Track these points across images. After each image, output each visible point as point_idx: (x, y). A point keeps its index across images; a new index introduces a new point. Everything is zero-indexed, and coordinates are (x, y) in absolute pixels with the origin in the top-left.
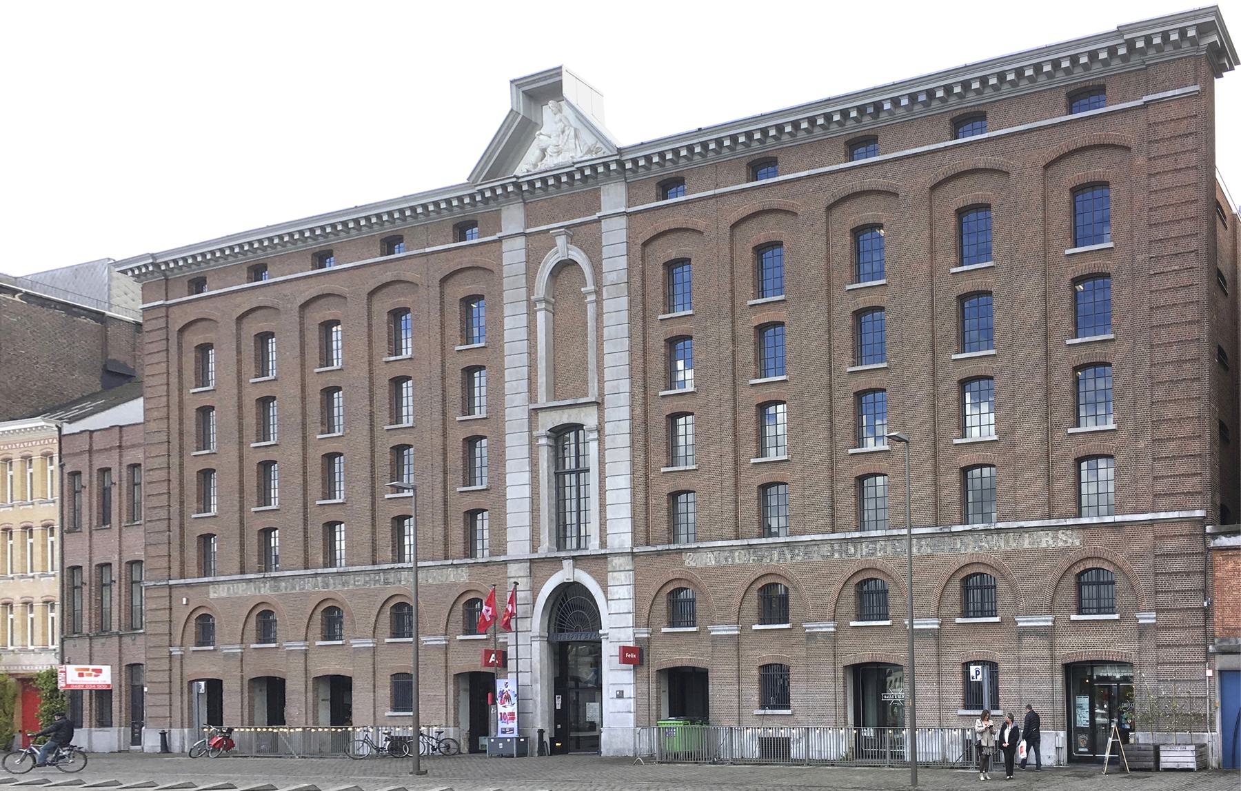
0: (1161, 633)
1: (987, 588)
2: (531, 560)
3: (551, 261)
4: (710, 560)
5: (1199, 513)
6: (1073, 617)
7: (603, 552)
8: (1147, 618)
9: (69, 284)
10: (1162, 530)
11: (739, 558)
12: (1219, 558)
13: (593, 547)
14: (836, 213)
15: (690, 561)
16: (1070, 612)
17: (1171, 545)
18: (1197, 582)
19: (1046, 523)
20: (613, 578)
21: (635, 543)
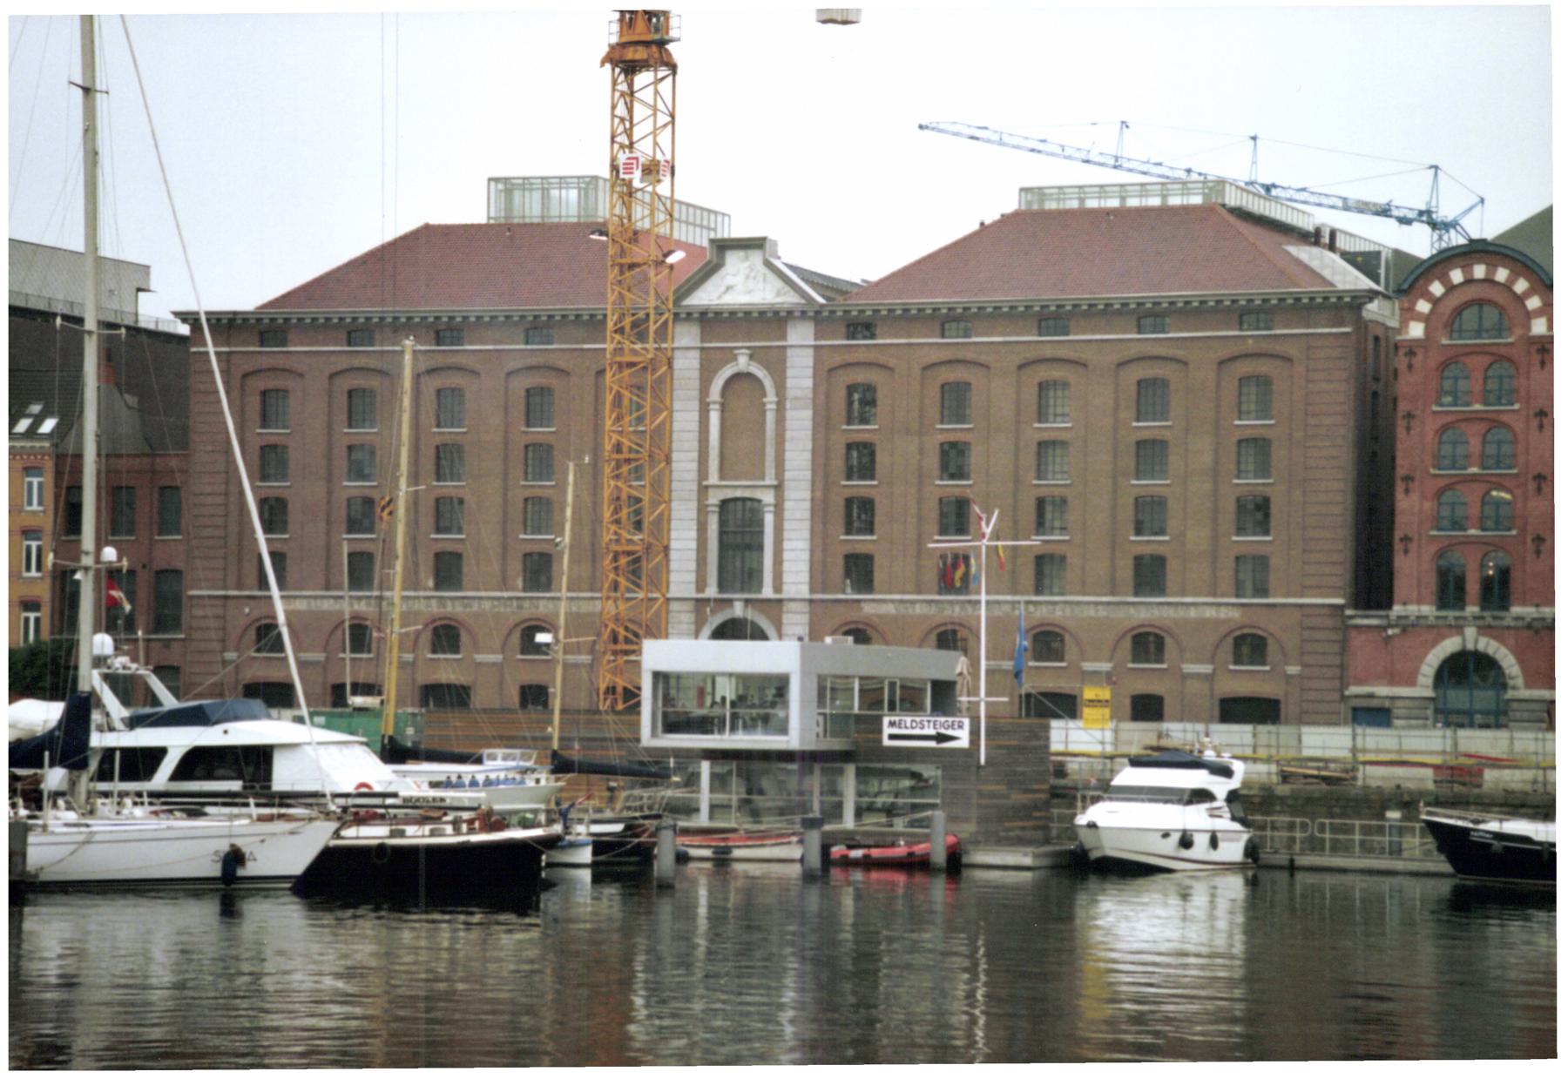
2: (698, 600)
3: (727, 372)
5: (1340, 601)
8: (1293, 669)
11: (919, 609)
12: (1353, 634)
13: (768, 592)
14: (1028, 371)
15: (868, 609)
17: (1314, 622)
20: (786, 618)
21: (812, 590)
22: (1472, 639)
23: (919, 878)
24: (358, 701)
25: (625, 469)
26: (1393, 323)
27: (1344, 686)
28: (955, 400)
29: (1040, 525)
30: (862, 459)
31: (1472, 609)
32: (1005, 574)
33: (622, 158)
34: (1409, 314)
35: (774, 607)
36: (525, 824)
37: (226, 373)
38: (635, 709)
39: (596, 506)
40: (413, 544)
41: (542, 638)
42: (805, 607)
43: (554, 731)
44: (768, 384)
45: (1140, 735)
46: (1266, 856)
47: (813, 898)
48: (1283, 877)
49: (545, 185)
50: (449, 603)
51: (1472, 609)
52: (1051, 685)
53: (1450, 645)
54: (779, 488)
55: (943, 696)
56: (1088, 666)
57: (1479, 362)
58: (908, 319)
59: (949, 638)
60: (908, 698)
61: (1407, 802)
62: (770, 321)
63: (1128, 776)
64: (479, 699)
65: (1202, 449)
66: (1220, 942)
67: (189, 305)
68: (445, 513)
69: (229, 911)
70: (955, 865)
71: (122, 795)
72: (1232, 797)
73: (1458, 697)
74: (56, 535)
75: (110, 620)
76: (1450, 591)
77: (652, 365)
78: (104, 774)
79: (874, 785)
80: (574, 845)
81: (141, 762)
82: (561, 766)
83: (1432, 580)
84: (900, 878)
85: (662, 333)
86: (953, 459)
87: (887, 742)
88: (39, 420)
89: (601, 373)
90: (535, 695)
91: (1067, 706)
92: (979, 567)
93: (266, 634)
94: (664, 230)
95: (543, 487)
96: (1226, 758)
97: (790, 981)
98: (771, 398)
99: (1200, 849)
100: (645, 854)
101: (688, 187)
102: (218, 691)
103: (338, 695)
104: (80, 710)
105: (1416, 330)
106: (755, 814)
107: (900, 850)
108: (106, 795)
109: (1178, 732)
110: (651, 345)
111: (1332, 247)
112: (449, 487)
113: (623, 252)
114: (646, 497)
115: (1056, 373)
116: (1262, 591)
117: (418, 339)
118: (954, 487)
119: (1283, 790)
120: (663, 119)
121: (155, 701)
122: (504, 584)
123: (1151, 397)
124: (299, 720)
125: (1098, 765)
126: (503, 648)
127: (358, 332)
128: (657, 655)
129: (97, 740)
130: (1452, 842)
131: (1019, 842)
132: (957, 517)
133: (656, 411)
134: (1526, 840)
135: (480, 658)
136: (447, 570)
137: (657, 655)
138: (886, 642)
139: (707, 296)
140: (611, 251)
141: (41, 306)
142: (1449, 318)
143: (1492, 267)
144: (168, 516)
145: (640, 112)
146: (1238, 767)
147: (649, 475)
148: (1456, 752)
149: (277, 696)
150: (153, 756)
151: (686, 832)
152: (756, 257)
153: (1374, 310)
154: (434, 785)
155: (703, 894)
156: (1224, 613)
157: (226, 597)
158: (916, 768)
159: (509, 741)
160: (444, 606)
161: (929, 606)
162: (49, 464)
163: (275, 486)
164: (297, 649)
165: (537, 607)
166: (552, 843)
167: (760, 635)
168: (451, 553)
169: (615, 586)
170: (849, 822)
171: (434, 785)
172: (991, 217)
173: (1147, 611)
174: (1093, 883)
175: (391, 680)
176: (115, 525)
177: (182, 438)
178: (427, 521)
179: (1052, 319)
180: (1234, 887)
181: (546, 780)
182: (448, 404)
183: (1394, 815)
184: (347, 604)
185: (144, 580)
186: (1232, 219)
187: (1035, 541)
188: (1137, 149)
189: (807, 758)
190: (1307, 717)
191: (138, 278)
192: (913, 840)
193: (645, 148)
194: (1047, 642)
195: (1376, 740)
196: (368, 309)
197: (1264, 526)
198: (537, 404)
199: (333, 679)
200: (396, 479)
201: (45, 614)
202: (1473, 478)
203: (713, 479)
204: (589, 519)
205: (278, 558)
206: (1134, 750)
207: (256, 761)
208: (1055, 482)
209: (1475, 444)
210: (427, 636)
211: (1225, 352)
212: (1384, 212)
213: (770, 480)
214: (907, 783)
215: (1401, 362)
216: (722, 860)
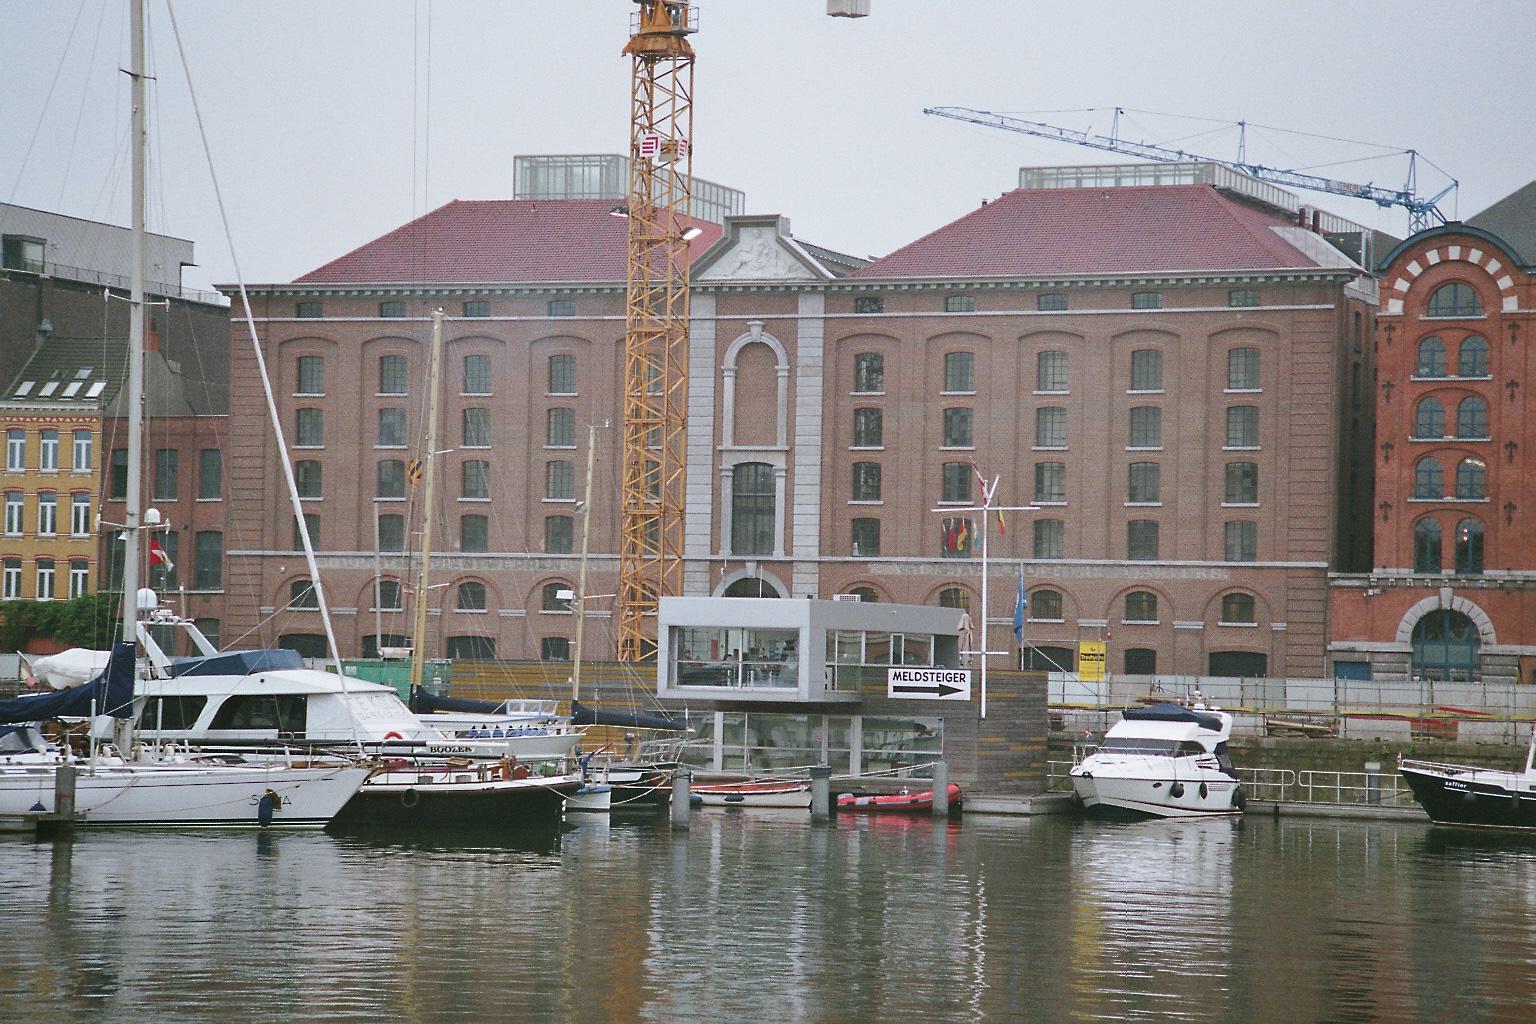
0: (1290, 637)
1: (1152, 601)
3: (742, 341)
4: (897, 570)
6: (1220, 624)
7: (788, 558)
8: (1278, 626)
9: (1314, 888)
10: (1292, 573)
12: (1336, 593)
13: (779, 554)
16: (1219, 620)
18: (1320, 606)
19: (1202, 563)
21: (821, 553)
22: (1447, 599)
23: (922, 823)
24: (389, 651)
28: (958, 368)
29: (1039, 492)
30: (870, 425)
31: (1448, 572)
32: (1004, 536)
34: (1388, 292)
36: (547, 773)
39: (615, 469)
40: (441, 508)
41: (562, 594)
42: (815, 568)
43: (574, 681)
44: (782, 366)
45: (1133, 687)
47: (821, 840)
49: (568, 162)
50: (474, 562)
51: (1448, 572)
52: (1048, 639)
53: (1427, 604)
55: (946, 649)
60: (914, 652)
61: (1387, 754)
62: (779, 296)
63: (1123, 729)
64: (503, 650)
66: (1209, 883)
68: (470, 477)
70: (956, 811)
72: (1221, 749)
73: (1434, 652)
74: (103, 498)
75: (153, 576)
76: (1427, 555)
78: (148, 723)
79: (880, 737)
81: (182, 711)
85: (679, 305)
86: (956, 425)
88: (87, 384)
90: (556, 647)
91: (1065, 659)
92: (980, 531)
93: (300, 589)
94: (680, 207)
97: (798, 916)
98: (782, 366)
99: (1191, 791)
100: (662, 800)
101: (705, 165)
102: (255, 642)
104: (125, 661)
105: (1395, 307)
107: (905, 798)
109: (1169, 685)
115: (1055, 344)
118: (957, 452)
119: (1269, 742)
122: (528, 545)
123: (1144, 365)
124: (332, 670)
125: (1093, 717)
127: (388, 304)
128: (672, 610)
130: (1427, 790)
135: (503, 612)
136: (473, 531)
137: (672, 610)
139: (722, 272)
142: (1423, 297)
145: (659, 96)
146: (1226, 719)
149: (311, 647)
150: (197, 703)
151: (699, 780)
152: (769, 234)
153: (1354, 287)
156: (1213, 575)
159: (531, 692)
160: (470, 566)
161: (933, 568)
162: (97, 427)
165: (559, 567)
166: (571, 789)
167: (771, 593)
169: (634, 548)
173: (1140, 572)
175: (420, 632)
176: (158, 488)
177: (223, 401)
178: (455, 484)
180: (1222, 832)
181: (566, 730)
184: (378, 563)
186: (1222, 200)
187: (1033, 507)
190: (1291, 671)
191: (183, 254)
193: (664, 128)
194: (1046, 600)
195: (1357, 693)
199: (363, 631)
203: (727, 444)
204: (609, 484)
206: (1127, 703)
207: (291, 710)
208: (1054, 448)
212: (1364, 194)
213: (781, 445)
216: (734, 808)
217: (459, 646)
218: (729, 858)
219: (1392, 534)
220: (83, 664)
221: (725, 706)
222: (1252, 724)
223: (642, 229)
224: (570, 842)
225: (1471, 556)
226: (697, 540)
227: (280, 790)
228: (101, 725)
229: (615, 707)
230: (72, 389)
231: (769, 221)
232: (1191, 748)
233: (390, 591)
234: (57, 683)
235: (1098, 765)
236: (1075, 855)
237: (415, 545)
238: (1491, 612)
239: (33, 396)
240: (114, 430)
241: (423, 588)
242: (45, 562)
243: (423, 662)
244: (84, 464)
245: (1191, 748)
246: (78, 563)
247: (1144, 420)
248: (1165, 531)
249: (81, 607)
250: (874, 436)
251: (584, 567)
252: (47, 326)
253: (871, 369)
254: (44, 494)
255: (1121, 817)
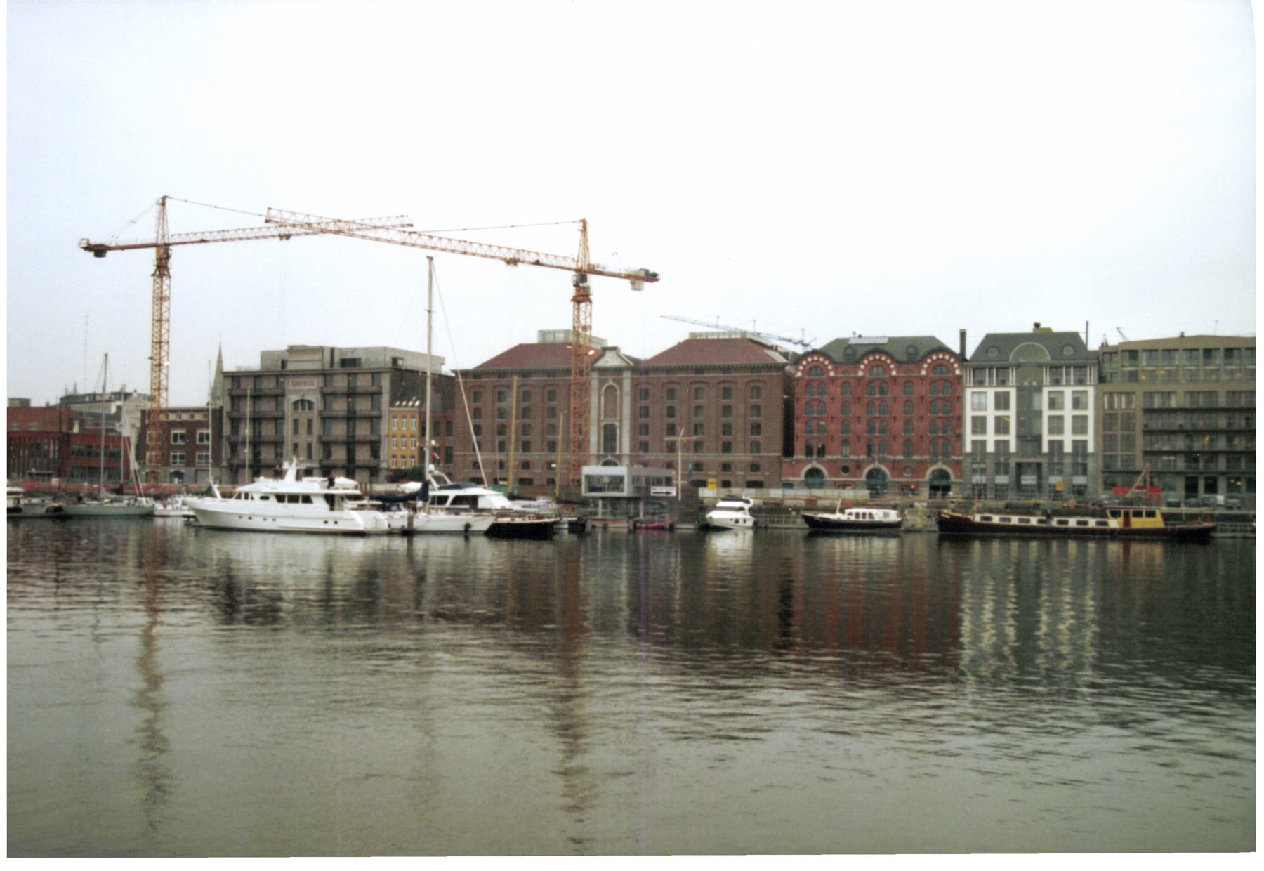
5: (779, 454)
22: (816, 465)
23: (661, 532)
24: (501, 483)
25: (577, 415)
26: (793, 372)
27: (781, 476)
28: (671, 394)
29: (696, 433)
30: (645, 412)
31: (815, 457)
32: (686, 446)
33: (576, 325)
34: (797, 370)
35: (620, 457)
36: (549, 518)
37: (465, 387)
38: (580, 485)
39: (569, 427)
40: (517, 440)
41: (554, 466)
43: (557, 491)
45: (724, 492)
46: (759, 524)
47: (631, 537)
48: (763, 530)
49: (554, 332)
51: (815, 457)
52: (699, 478)
53: (809, 466)
54: (621, 421)
55: (668, 481)
56: (710, 473)
57: (815, 384)
58: (657, 370)
59: (670, 465)
60: (658, 482)
61: (797, 509)
62: (617, 371)
63: (721, 504)
64: (536, 482)
65: (741, 407)
66: (746, 548)
67: (455, 368)
68: (525, 429)
69: (467, 538)
70: (672, 528)
71: (438, 509)
72: (750, 509)
73: (811, 480)
74: (420, 438)
75: (434, 461)
76: (809, 452)
77: (585, 383)
78: (433, 503)
79: (648, 507)
80: (563, 523)
81: (442, 500)
82: (559, 501)
83: (804, 448)
84: (656, 532)
85: (588, 374)
86: (671, 412)
87: (652, 494)
88: (415, 402)
89: (570, 386)
90: (552, 482)
91: (704, 484)
92: (679, 445)
93: (476, 465)
94: (588, 345)
95: (552, 421)
96: (748, 498)
97: (624, 565)
98: (618, 393)
99: (741, 523)
100: (583, 526)
101: (596, 332)
102: (463, 480)
103: (495, 481)
104: (426, 485)
105: (799, 374)
106: (614, 515)
107: (656, 524)
108: (433, 509)
109: (735, 491)
110: (584, 378)
111: (776, 350)
112: (527, 421)
113: (576, 351)
114: (583, 423)
115: (701, 385)
116: (758, 451)
117: (519, 376)
118: (671, 420)
119: (764, 507)
120: (588, 315)
121: (445, 482)
122: (542, 450)
123: (727, 393)
124: (485, 488)
125: (712, 501)
126: (542, 469)
127: (501, 374)
128: (587, 470)
129: (431, 493)
130: (809, 520)
131: (689, 522)
132: (672, 430)
133: (586, 397)
134: (829, 519)
136: (526, 447)
137: (587, 470)
138: (652, 466)
139: (601, 363)
140: (573, 351)
141: (415, 369)
142: (808, 371)
143: (819, 357)
144: (449, 431)
145: (581, 313)
146: (752, 501)
147: (584, 416)
148: (811, 496)
149: (478, 481)
150: (446, 498)
151: (595, 520)
152: (614, 352)
153: (788, 368)
154: (524, 507)
155: (600, 537)
157: (1075, 359)
158: (661, 502)
159: (544, 494)
161: (664, 457)
162: (417, 416)
163: (477, 421)
164: (484, 468)
166: (555, 523)
167: (615, 464)
168: (605, 432)
169: (574, 451)
170: (641, 517)
171: (524, 507)
172: (681, 340)
173: (726, 458)
174: (710, 532)
175: (511, 477)
176: (435, 434)
177: (453, 407)
178: (520, 432)
179: (700, 370)
180: (750, 533)
181: (554, 506)
182: (526, 396)
183: (794, 513)
184: (498, 456)
185: (443, 450)
186: (749, 343)
187: (694, 438)
188: (722, 323)
189: (629, 499)
190: (771, 486)
191: (441, 361)
192: (659, 522)
193: (583, 322)
194: (698, 466)
195: (789, 492)
196: (502, 368)
197: (758, 433)
198: (552, 396)
199: (494, 476)
200: (511, 419)
201: (416, 459)
202: (815, 418)
203: (602, 418)
204: (567, 431)
205: (479, 443)
206: (723, 496)
207: (473, 500)
208: (701, 419)
209: (815, 408)
210: (520, 466)
211: (747, 380)
212: (790, 341)
213: (618, 418)
214: (657, 506)
215: (795, 383)
216: (605, 528)
217: (522, 481)
218: (604, 544)
219: (799, 445)
220: (414, 486)
221: (603, 499)
222: (759, 502)
223: (576, 351)
224: (556, 537)
225: (822, 452)
226: (593, 449)
227: (470, 522)
228: (420, 504)
229: (570, 498)
230: (411, 403)
231: (614, 349)
232: (741, 509)
233: (502, 465)
234: (407, 492)
235: (715, 515)
236: (707, 539)
237: (509, 451)
238: (828, 469)
239: (400, 406)
240: (422, 416)
241: (512, 463)
242: (403, 457)
243: (511, 484)
244: (414, 429)
245: (741, 509)
246: (413, 457)
247: (727, 410)
248: (734, 445)
249: (413, 470)
250: (647, 415)
251: (559, 457)
252: (404, 384)
253: (646, 394)
254: (403, 436)
255: (721, 529)
